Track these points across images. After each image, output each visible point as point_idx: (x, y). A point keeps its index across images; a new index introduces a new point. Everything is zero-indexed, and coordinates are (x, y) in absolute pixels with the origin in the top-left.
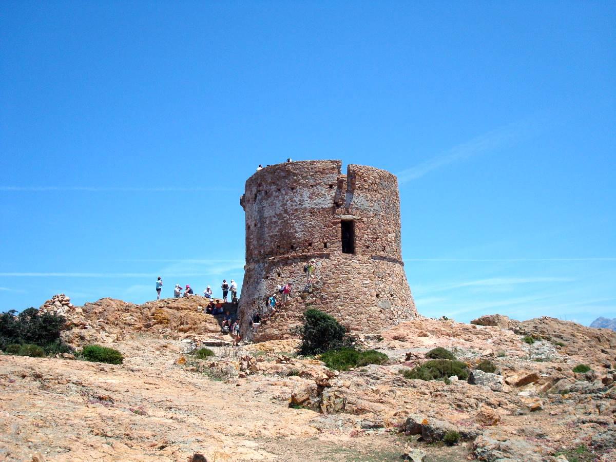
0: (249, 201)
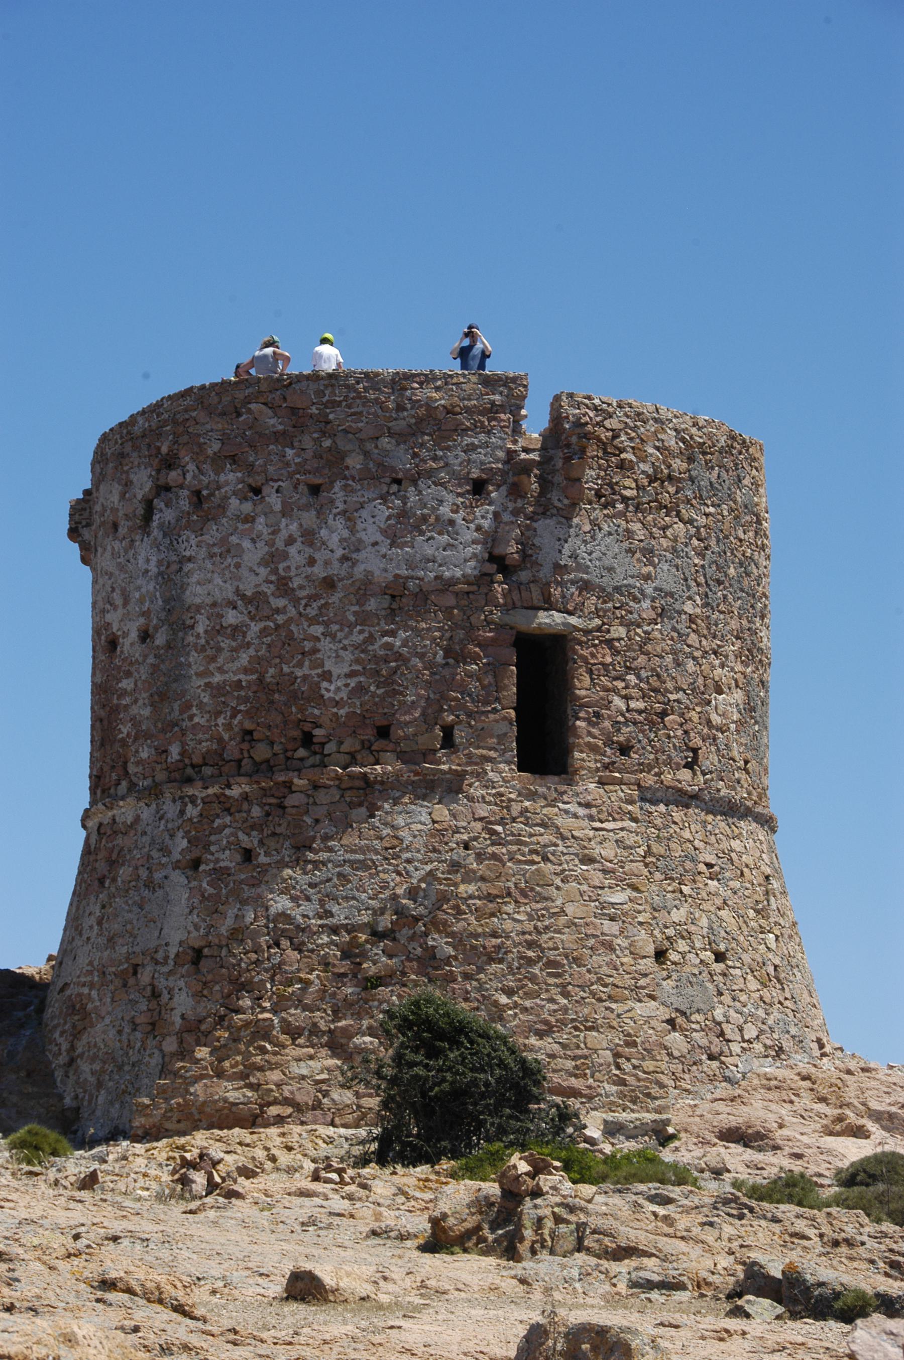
0: (115, 526)
